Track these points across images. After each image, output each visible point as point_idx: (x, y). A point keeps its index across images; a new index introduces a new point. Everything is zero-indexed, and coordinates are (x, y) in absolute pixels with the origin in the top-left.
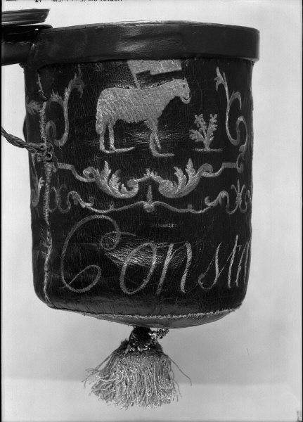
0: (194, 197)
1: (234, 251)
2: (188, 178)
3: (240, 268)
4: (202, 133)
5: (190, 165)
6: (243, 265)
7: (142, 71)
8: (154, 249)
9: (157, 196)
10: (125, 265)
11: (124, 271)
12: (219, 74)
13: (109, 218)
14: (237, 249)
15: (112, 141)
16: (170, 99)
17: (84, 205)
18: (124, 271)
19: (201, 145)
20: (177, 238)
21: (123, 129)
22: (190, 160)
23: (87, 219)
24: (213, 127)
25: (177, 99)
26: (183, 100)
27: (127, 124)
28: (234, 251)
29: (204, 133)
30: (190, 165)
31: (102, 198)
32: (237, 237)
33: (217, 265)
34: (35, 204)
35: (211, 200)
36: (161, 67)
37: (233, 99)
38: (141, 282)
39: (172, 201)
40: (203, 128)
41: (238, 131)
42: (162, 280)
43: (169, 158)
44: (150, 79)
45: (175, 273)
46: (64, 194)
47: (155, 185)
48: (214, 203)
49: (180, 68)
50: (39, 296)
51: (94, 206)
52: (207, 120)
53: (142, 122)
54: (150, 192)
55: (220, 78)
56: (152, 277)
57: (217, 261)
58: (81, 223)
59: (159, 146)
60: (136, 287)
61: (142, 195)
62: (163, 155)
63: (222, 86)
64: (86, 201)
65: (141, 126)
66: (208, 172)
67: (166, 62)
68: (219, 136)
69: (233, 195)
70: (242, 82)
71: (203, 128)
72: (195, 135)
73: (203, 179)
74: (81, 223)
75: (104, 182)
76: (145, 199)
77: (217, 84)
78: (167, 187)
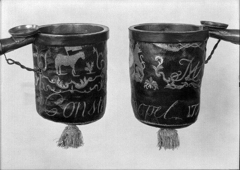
0: (87, 88)
1: (100, 102)
2: (84, 82)
3: (102, 106)
4: (89, 68)
5: (85, 79)
6: (103, 106)
7: (69, 50)
8: (74, 104)
9: (74, 88)
10: (65, 109)
11: (64, 111)
12: (94, 49)
13: (59, 94)
14: (101, 101)
15: (60, 72)
16: (78, 58)
17: (52, 90)
18: (64, 111)
19: (89, 72)
20: (81, 100)
21: (63, 68)
22: (85, 77)
23: (53, 94)
24: (92, 66)
25: (81, 58)
26: (83, 59)
27: (65, 66)
28: (100, 102)
29: (89, 68)
30: (85, 79)
31: (57, 88)
32: (101, 97)
33: (94, 107)
34: (36, 85)
35: (92, 88)
36: (75, 49)
37: (99, 55)
38: (70, 114)
39: (79, 90)
40: (89, 66)
41: (101, 65)
42: (76, 113)
43: (78, 77)
44: (71, 53)
45: (80, 111)
46: (45, 86)
47: (74, 85)
48: (93, 89)
49: (81, 49)
50: (38, 112)
51: (55, 91)
52: (90, 64)
53: (69, 66)
54: (72, 87)
55: (95, 50)
56: (73, 113)
57: (94, 106)
58: (51, 95)
59: (75, 73)
60: (68, 115)
61: (70, 88)
62: (76, 76)
63: (95, 52)
64: (53, 89)
65: (69, 67)
66: (90, 80)
67: (77, 47)
68: (95, 69)
69: (99, 85)
70: (102, 48)
71: (89, 66)
72: (86, 69)
73: (89, 82)
74: (51, 95)
75: (58, 83)
76: (71, 89)
77: (94, 52)
78: (78, 85)
